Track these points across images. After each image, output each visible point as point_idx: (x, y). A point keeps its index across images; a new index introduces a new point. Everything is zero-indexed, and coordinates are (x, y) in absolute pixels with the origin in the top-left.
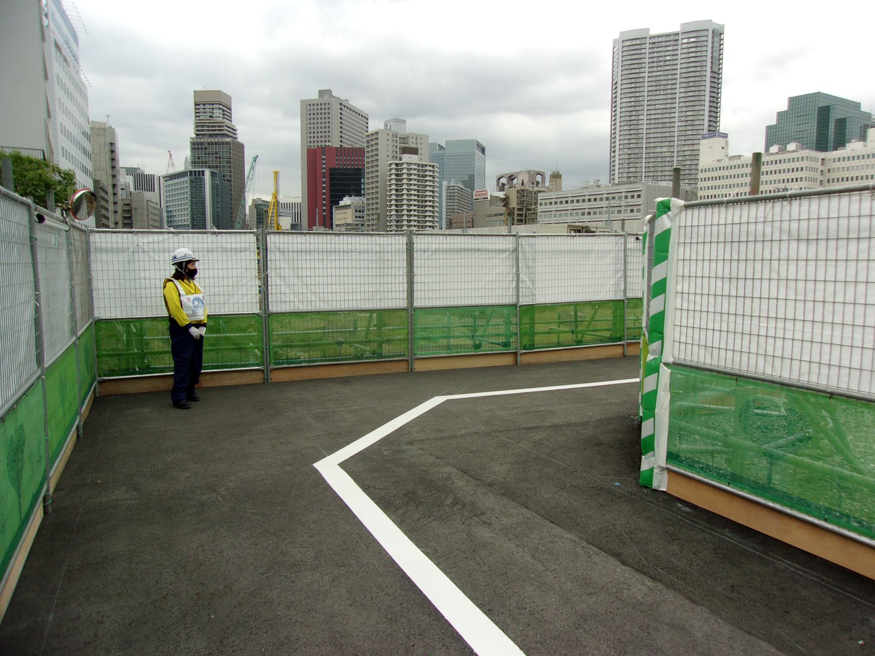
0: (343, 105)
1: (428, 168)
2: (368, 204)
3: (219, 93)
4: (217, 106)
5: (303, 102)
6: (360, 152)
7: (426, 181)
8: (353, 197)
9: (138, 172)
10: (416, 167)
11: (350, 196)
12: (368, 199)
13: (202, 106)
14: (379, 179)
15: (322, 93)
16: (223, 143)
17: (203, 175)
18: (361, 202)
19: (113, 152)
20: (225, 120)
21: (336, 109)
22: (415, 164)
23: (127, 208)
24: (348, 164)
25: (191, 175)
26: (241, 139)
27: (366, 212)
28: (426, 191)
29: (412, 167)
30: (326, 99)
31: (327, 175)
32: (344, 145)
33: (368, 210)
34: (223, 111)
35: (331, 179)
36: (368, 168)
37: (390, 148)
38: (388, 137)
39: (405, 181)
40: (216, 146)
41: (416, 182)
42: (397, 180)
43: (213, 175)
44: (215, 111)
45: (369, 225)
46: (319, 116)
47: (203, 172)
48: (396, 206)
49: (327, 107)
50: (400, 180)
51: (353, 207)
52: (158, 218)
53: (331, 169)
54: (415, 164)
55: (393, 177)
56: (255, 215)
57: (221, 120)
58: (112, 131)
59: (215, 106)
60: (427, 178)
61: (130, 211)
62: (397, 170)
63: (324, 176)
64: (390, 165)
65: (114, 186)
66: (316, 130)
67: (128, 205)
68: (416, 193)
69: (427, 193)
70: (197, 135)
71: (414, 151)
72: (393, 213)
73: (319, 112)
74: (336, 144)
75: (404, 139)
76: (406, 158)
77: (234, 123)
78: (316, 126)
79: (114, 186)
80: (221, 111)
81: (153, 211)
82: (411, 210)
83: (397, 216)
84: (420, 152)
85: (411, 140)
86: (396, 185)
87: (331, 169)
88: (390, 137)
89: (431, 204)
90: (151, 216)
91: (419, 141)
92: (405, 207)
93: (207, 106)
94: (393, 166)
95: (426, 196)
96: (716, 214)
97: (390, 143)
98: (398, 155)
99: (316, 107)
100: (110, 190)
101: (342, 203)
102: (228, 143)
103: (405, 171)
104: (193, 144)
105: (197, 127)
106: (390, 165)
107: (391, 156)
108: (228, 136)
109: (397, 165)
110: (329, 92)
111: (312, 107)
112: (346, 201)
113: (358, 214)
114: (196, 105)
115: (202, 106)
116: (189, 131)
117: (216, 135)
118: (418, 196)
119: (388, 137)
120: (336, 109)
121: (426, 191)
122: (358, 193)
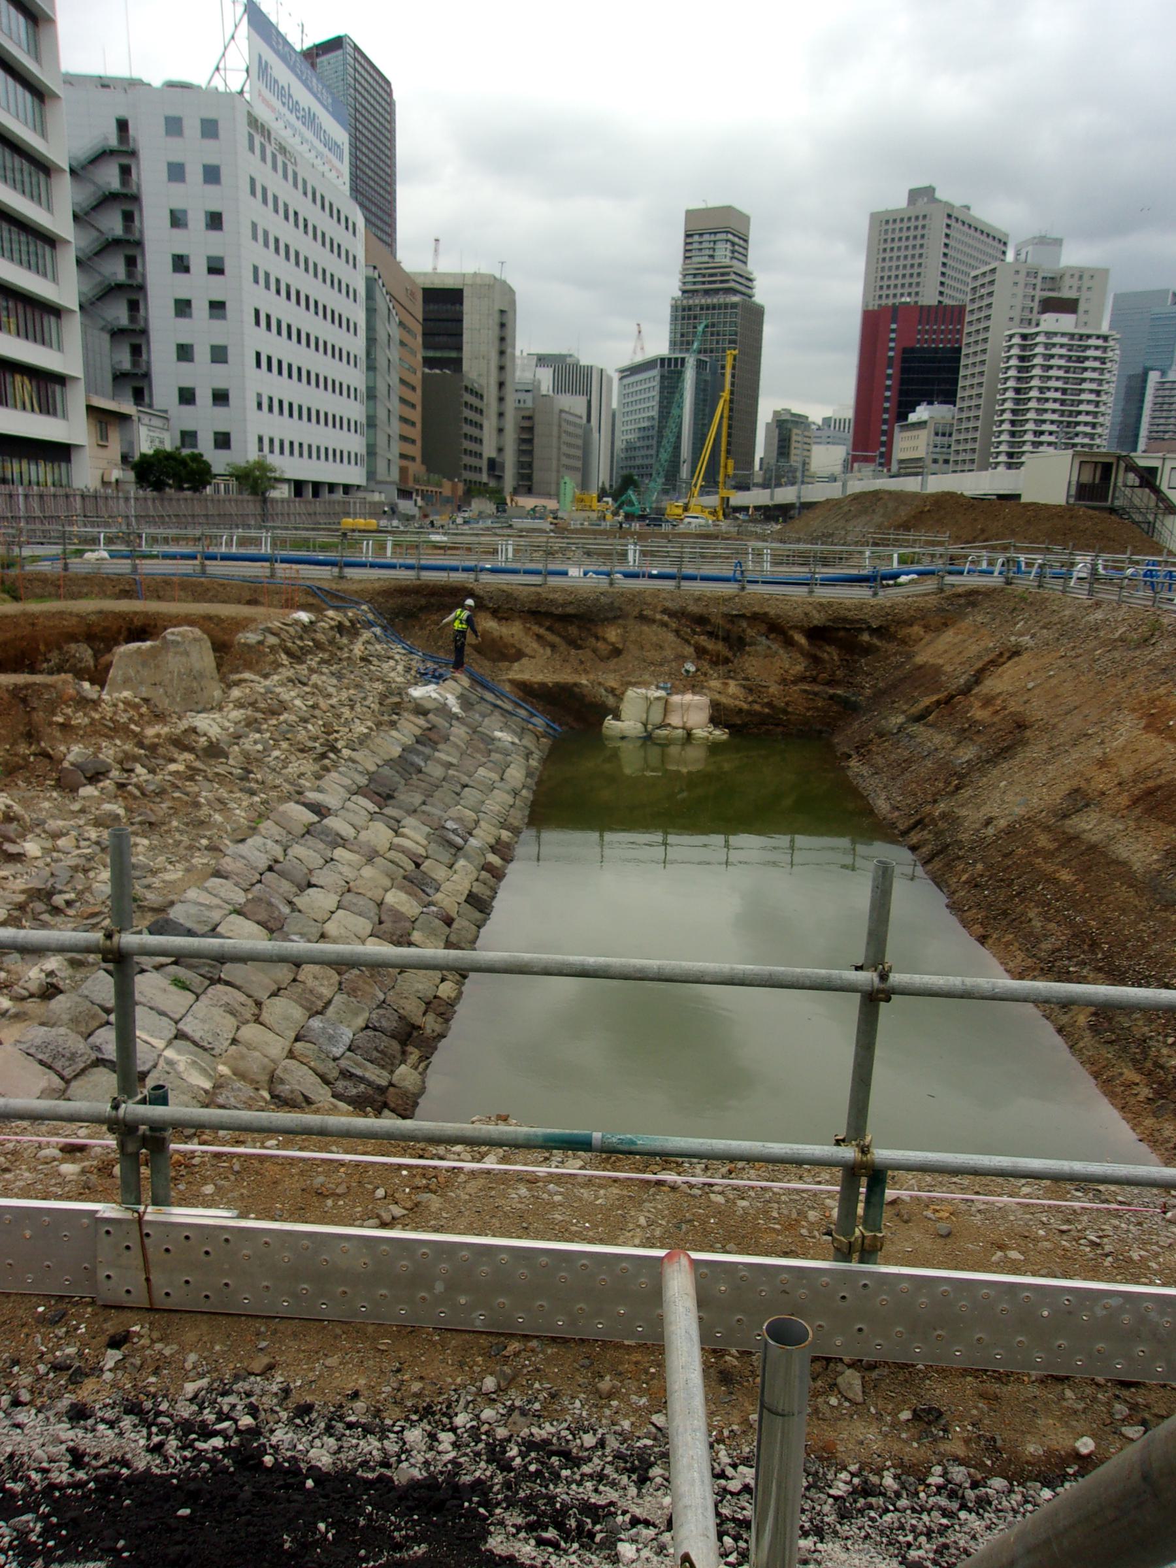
0: (955, 218)
1: (1091, 342)
2: (960, 420)
3: (728, 210)
4: (723, 236)
5: (874, 216)
6: (956, 314)
7: (1085, 369)
8: (936, 406)
9: (569, 360)
10: (1065, 340)
11: (930, 403)
12: (961, 410)
13: (696, 238)
14: (985, 368)
15: (915, 195)
16: (726, 306)
17: (683, 364)
18: (949, 416)
19: (503, 325)
20: (735, 262)
21: (937, 225)
22: (1063, 335)
23: (526, 424)
24: (927, 338)
25: (662, 365)
26: (759, 298)
27: (954, 437)
28: (1082, 391)
29: (1056, 340)
30: (922, 206)
31: (897, 363)
32: (947, 301)
33: (959, 431)
34: (733, 244)
35: (904, 370)
36: (968, 345)
37: (1018, 302)
38: (1018, 278)
39: (1036, 372)
40: (717, 311)
41: (1061, 373)
42: (1020, 369)
43: (700, 365)
44: (719, 245)
45: (956, 462)
46: (903, 244)
47: (683, 359)
48: (1013, 423)
49: (920, 223)
50: (1027, 369)
51: (931, 428)
52: (580, 442)
53: (905, 351)
54: (1063, 335)
55: (1014, 362)
56: (776, 441)
57: (727, 261)
58: (509, 292)
59: (719, 237)
60: (1087, 364)
61: (531, 429)
62: (1023, 348)
63: (890, 363)
64: (1011, 337)
65: (501, 385)
66: (893, 273)
67: (530, 418)
68: (1058, 395)
69: (1083, 397)
70: (684, 292)
71: (1069, 306)
72: (1005, 437)
73: (904, 234)
74: (929, 298)
75: (1053, 281)
76: (1050, 321)
77: (751, 266)
78: (894, 264)
79: (501, 385)
80: (729, 246)
81: (571, 429)
82: (1042, 433)
83: (1011, 444)
84: (1082, 307)
85: (1067, 282)
86: (1019, 379)
87: (905, 351)
88: (1021, 278)
89: (1089, 419)
90: (565, 438)
91: (1086, 283)
92: (1030, 426)
93: (706, 237)
94: (1016, 340)
95: (1081, 402)
96: (49, 469)
97: (1020, 291)
98: (1035, 316)
99: (898, 226)
100: (491, 394)
101: (913, 418)
102: (734, 306)
103: (1039, 350)
104: (675, 308)
105: (685, 276)
106: (1011, 337)
107: (1017, 320)
108: (734, 291)
109: (1024, 337)
110: (929, 192)
111: (890, 227)
112: (922, 413)
113: (524, 447)
114: (688, 236)
115: (696, 238)
116: (671, 286)
117: (717, 291)
118: (1063, 402)
119: (1018, 278)
120: (937, 225)
121: (1082, 391)
122: (949, 397)
